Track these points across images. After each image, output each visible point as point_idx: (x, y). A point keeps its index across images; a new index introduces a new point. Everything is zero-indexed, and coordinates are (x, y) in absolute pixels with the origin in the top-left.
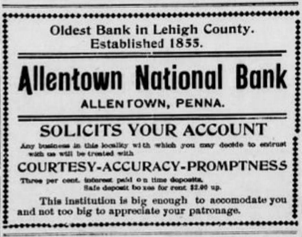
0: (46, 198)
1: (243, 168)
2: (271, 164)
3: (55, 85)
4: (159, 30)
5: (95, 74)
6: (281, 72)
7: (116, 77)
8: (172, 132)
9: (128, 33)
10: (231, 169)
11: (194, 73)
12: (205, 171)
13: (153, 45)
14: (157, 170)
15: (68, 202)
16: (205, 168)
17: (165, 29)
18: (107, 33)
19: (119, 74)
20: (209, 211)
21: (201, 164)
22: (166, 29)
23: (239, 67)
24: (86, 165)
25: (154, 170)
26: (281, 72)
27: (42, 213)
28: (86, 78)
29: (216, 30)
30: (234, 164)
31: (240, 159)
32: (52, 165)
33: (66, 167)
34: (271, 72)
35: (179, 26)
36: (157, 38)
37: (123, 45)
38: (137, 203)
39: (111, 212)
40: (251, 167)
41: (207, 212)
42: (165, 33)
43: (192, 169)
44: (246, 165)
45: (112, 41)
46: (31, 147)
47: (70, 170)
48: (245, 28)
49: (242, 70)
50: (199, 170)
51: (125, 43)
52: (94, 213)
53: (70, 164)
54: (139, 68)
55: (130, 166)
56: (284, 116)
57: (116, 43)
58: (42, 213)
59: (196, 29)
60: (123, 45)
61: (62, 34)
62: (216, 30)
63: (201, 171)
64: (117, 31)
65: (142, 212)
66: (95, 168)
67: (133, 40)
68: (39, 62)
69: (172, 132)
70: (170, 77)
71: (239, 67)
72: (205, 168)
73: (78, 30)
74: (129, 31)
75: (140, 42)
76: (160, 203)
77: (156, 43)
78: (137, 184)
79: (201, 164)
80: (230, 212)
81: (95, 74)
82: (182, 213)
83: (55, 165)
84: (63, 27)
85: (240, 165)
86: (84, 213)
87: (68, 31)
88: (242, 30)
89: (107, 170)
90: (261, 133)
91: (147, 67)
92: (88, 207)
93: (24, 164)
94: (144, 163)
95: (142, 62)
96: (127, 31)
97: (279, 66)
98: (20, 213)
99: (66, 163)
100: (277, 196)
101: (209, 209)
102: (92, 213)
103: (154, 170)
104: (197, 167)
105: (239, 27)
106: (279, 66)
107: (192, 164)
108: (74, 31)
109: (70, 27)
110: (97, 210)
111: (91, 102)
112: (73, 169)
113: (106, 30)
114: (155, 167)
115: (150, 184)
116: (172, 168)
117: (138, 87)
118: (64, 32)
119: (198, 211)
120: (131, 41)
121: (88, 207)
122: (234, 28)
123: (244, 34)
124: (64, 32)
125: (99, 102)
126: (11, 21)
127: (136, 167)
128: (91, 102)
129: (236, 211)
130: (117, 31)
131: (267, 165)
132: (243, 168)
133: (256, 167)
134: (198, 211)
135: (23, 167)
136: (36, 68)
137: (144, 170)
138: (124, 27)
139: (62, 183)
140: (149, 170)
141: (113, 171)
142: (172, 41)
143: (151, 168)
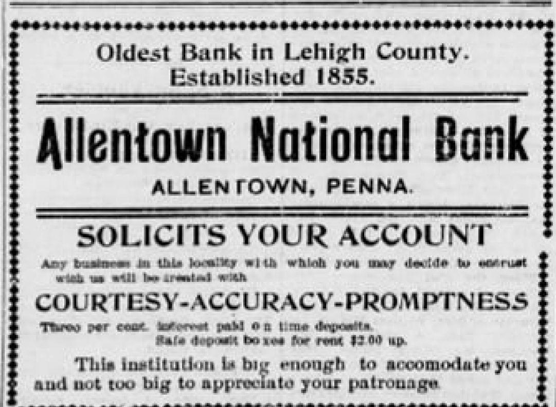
1: (447, 306)
3: (104, 153)
4: (295, 52)
22: (310, 51)
23: (441, 121)
27: (79, 386)
29: (399, 54)
33: (124, 302)
34: (499, 131)
36: (293, 67)
37: (229, 79)
39: (206, 385)
40: (463, 304)
42: (307, 58)
44: (453, 301)
45: (209, 73)
47: (130, 307)
48: (452, 50)
52: (174, 385)
53: (131, 297)
54: (256, 122)
55: (241, 299)
57: (217, 77)
58: (79, 386)
59: (362, 50)
60: (229, 79)
61: (118, 59)
62: (399, 54)
67: (247, 71)
68: (75, 112)
71: (441, 121)
74: (240, 53)
75: (260, 75)
77: (288, 76)
80: (424, 386)
85: (442, 300)
88: (448, 54)
92: (163, 376)
95: (263, 111)
97: (513, 120)
98: (39, 386)
99: (123, 295)
102: (171, 386)
104: (362, 303)
106: (513, 120)
107: (354, 298)
110: (181, 381)
111: (170, 183)
112: (136, 305)
113: (197, 51)
116: (319, 304)
117: (255, 157)
119: (364, 385)
121: (163, 376)
123: (451, 62)
125: (186, 183)
127: (252, 302)
128: (170, 183)
129: (434, 384)
132: (447, 306)
134: (364, 385)
135: (45, 303)
136: (69, 121)
143: (278, 305)
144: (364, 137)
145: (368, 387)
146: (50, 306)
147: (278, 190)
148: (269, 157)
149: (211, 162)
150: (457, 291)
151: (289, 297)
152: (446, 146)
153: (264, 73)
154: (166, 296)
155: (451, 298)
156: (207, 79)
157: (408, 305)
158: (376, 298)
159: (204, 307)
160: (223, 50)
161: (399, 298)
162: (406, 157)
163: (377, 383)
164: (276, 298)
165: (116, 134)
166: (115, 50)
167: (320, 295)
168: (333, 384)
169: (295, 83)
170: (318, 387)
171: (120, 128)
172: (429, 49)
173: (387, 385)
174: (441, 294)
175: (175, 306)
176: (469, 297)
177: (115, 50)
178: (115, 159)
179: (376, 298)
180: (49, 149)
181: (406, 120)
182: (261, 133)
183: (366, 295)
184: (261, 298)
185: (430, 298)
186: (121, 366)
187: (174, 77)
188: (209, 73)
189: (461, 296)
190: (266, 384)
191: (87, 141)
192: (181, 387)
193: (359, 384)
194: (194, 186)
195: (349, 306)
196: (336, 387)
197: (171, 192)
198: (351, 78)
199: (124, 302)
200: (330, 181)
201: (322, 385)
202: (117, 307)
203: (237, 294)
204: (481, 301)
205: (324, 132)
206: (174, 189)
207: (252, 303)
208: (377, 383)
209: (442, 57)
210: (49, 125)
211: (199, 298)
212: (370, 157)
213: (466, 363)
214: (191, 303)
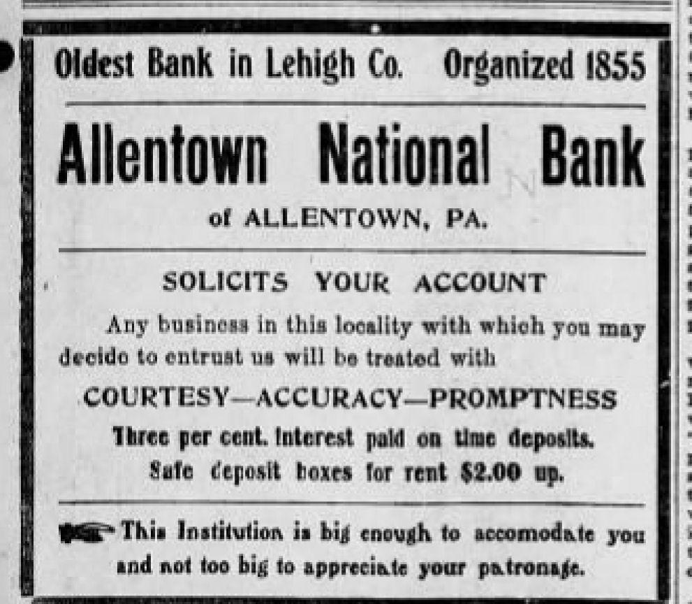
1: (538, 405)
2: (200, 394)
3: (136, 169)
5: (215, 141)
6: (633, 143)
7: (257, 148)
8: (382, 286)
10: (514, 404)
11: (435, 142)
12: (463, 407)
14: (359, 405)
16: (465, 402)
17: (553, 63)
19: (262, 142)
20: (521, 570)
21: (458, 395)
23: (548, 130)
24: (213, 395)
25: (354, 405)
26: (633, 143)
28: (197, 148)
30: (519, 395)
32: (340, 395)
33: (174, 396)
34: (611, 144)
38: (269, 540)
40: (554, 400)
41: (517, 573)
43: (438, 404)
44: (544, 399)
46: (634, 334)
47: (182, 403)
49: (554, 137)
50: (452, 406)
53: (182, 390)
54: (325, 129)
55: (309, 396)
63: (457, 408)
65: (370, 570)
66: (400, 402)
68: (102, 116)
69: (382, 286)
70: (390, 149)
71: (548, 130)
72: (465, 402)
79: (458, 395)
81: (215, 141)
82: (461, 573)
83: (154, 393)
85: (531, 397)
86: (254, 571)
89: (263, 404)
90: (537, 289)
91: (343, 128)
93: (96, 390)
94: (144, 390)
95: (333, 117)
97: (627, 130)
99: (173, 388)
100: (64, 519)
103: (354, 405)
104: (448, 400)
106: (627, 130)
107: (439, 395)
111: (266, 212)
112: (187, 400)
114: (356, 400)
115: (504, 453)
116: (389, 402)
117: (324, 178)
125: (285, 212)
127: (321, 398)
128: (266, 212)
131: (581, 398)
132: (538, 405)
133: (561, 401)
135: (93, 397)
136: (96, 128)
137: (335, 404)
139: (417, 448)
140: (345, 405)
141: (370, 408)
143: (349, 401)
144: (156, 150)
146: (100, 400)
147: (389, 224)
148: (342, 179)
149: (149, 184)
150: (548, 387)
151: (360, 394)
152: (555, 163)
154: (217, 390)
155: (171, 393)
158: (463, 394)
159: (364, 405)
161: (486, 395)
162: (486, 180)
164: (346, 394)
165: (149, 144)
167: (390, 392)
171: (154, 136)
174: (531, 390)
175: (226, 401)
176: (560, 394)
178: (149, 177)
179: (463, 394)
180: (70, 166)
182: (331, 145)
183: (453, 392)
184: (331, 394)
185: (519, 395)
189: (553, 392)
191: (242, 157)
194: (295, 216)
195: (433, 405)
197: (267, 224)
199: (174, 396)
200: (450, 212)
202: (167, 402)
203: (305, 390)
204: (572, 398)
205: (397, 142)
206: (271, 220)
207: (321, 399)
210: (71, 133)
211: (265, 393)
212: (397, 178)
214: (258, 398)
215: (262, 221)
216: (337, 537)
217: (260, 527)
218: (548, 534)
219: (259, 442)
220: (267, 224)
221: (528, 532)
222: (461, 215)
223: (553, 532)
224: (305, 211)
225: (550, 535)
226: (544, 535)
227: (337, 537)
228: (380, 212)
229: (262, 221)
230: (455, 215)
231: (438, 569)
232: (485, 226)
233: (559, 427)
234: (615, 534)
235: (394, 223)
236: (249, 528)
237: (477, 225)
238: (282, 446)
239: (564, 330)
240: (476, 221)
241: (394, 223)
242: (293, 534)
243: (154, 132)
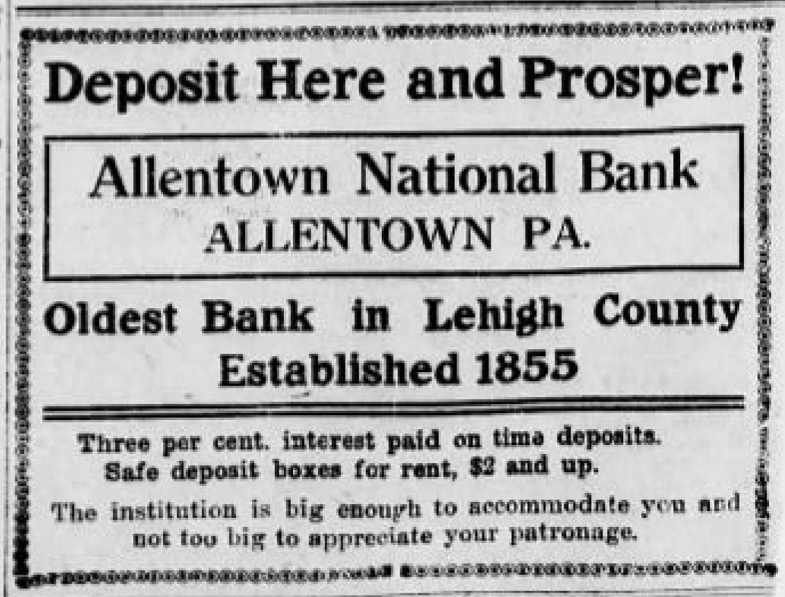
0: (346, 535)
4: (445, 313)
9: (308, 327)
13: (418, 373)
15: (119, 514)
18: (241, 328)
22: (471, 314)
29: (634, 313)
31: (353, 501)
35: (509, 301)
36: (434, 349)
42: (463, 327)
45: (285, 361)
48: (726, 305)
51: (327, 366)
56: (50, 414)
57: (301, 368)
59: (558, 309)
60: (323, 374)
61: (84, 330)
62: (634, 313)
64: (272, 319)
67: (355, 356)
73: (136, 317)
74: (310, 317)
76: (229, 517)
77: (427, 368)
78: (288, 527)
84: (83, 306)
87: (104, 322)
88: (718, 311)
96: (302, 317)
101: (362, 536)
105: (710, 302)
108: (124, 319)
109: (111, 307)
113: (234, 315)
118: (90, 327)
120: (348, 359)
122: (694, 304)
123: (724, 329)
124: (90, 327)
126: (53, 272)
129: (626, 533)
130: (272, 319)
138: (293, 304)
142: (484, 359)
145: (408, 542)
153: (383, 362)
156: (283, 372)
157: (283, 173)
160: (279, 313)
163: (548, 533)
166: (77, 311)
168: (488, 536)
169: (441, 379)
170: (198, 544)
172: (272, 312)
173: (564, 535)
177: (77, 311)
181: (549, 157)
186: (226, 540)
187: (226, 371)
188: (285, 361)
190: (396, 538)
192: (280, 543)
193: (460, 535)
194: (284, 234)
196: (492, 539)
197: (243, 248)
198: (544, 369)
200: (529, 222)
201: (203, 541)
208: (548, 533)
209: (711, 319)
213: (400, 535)
215: (235, 244)
216: (304, 514)
217: (208, 506)
218: (201, 540)
219: (446, 474)
220: (243, 248)
221: (529, 504)
222: (547, 226)
223: (210, 476)
224: (297, 224)
225: (203, 541)
226: (371, 512)
227: (304, 514)
228: (421, 223)
229: (235, 244)
230: (537, 226)
231: (465, 536)
232: (587, 245)
233: (690, 18)
234: (649, 503)
235: (289, 188)
236: (194, 507)
237: (576, 244)
238: (713, 512)
239: (654, 508)
240: (573, 236)
241: (289, 188)
242: (251, 511)
243: (144, 202)
